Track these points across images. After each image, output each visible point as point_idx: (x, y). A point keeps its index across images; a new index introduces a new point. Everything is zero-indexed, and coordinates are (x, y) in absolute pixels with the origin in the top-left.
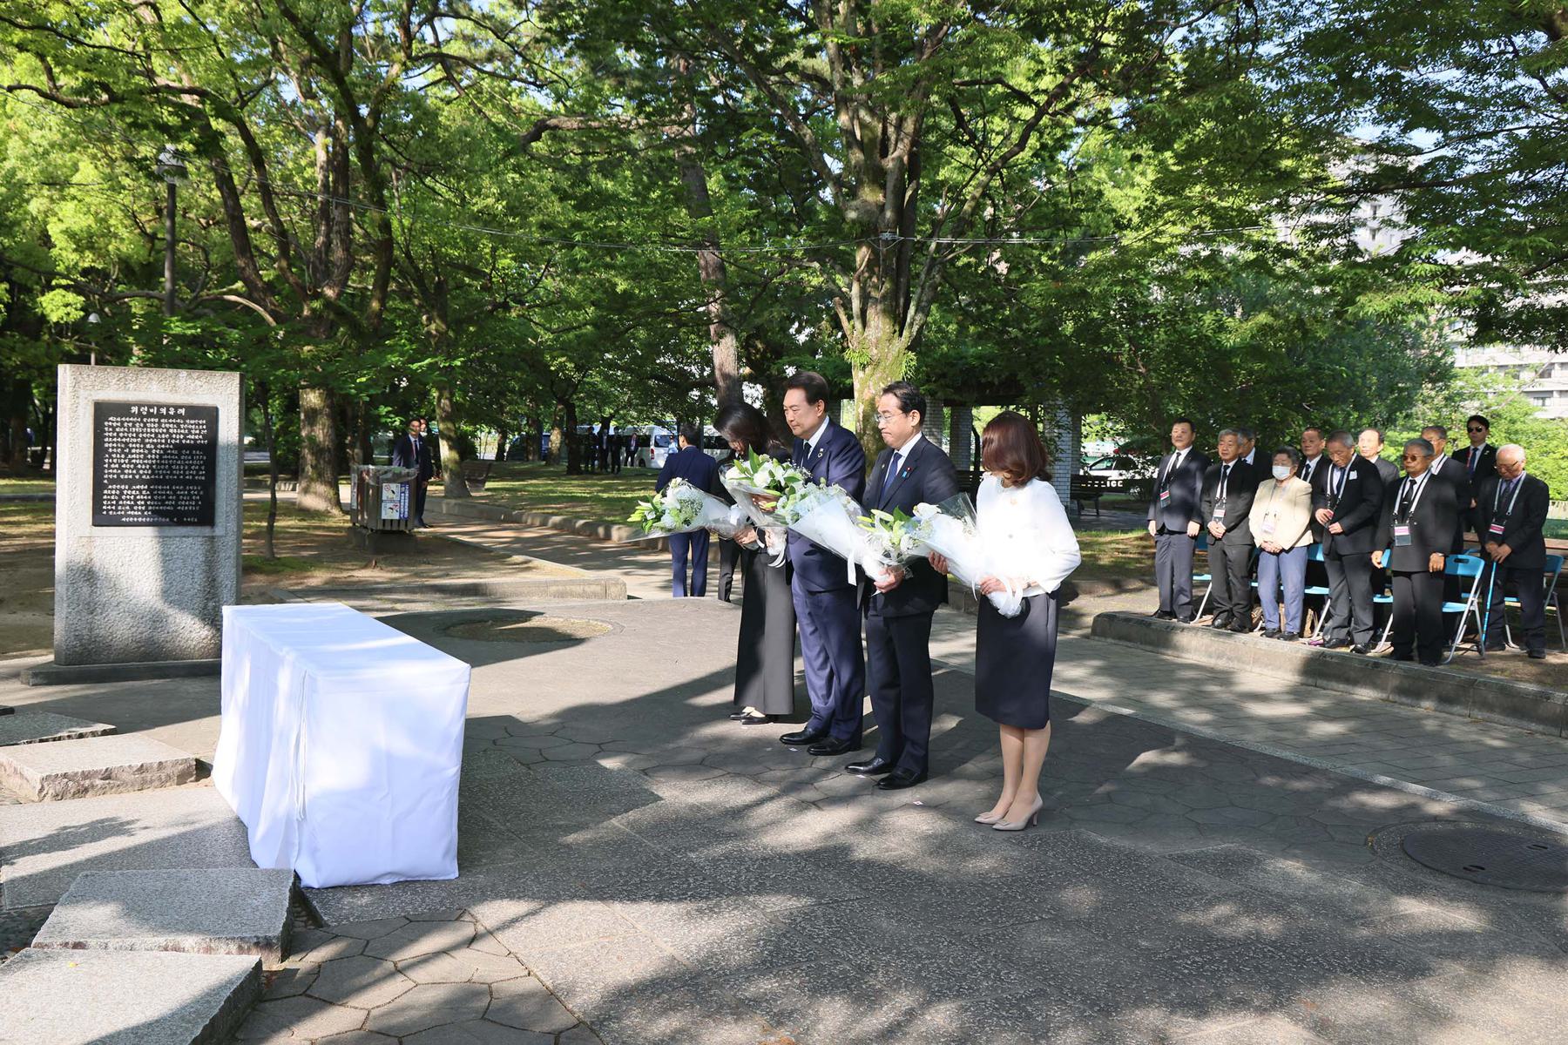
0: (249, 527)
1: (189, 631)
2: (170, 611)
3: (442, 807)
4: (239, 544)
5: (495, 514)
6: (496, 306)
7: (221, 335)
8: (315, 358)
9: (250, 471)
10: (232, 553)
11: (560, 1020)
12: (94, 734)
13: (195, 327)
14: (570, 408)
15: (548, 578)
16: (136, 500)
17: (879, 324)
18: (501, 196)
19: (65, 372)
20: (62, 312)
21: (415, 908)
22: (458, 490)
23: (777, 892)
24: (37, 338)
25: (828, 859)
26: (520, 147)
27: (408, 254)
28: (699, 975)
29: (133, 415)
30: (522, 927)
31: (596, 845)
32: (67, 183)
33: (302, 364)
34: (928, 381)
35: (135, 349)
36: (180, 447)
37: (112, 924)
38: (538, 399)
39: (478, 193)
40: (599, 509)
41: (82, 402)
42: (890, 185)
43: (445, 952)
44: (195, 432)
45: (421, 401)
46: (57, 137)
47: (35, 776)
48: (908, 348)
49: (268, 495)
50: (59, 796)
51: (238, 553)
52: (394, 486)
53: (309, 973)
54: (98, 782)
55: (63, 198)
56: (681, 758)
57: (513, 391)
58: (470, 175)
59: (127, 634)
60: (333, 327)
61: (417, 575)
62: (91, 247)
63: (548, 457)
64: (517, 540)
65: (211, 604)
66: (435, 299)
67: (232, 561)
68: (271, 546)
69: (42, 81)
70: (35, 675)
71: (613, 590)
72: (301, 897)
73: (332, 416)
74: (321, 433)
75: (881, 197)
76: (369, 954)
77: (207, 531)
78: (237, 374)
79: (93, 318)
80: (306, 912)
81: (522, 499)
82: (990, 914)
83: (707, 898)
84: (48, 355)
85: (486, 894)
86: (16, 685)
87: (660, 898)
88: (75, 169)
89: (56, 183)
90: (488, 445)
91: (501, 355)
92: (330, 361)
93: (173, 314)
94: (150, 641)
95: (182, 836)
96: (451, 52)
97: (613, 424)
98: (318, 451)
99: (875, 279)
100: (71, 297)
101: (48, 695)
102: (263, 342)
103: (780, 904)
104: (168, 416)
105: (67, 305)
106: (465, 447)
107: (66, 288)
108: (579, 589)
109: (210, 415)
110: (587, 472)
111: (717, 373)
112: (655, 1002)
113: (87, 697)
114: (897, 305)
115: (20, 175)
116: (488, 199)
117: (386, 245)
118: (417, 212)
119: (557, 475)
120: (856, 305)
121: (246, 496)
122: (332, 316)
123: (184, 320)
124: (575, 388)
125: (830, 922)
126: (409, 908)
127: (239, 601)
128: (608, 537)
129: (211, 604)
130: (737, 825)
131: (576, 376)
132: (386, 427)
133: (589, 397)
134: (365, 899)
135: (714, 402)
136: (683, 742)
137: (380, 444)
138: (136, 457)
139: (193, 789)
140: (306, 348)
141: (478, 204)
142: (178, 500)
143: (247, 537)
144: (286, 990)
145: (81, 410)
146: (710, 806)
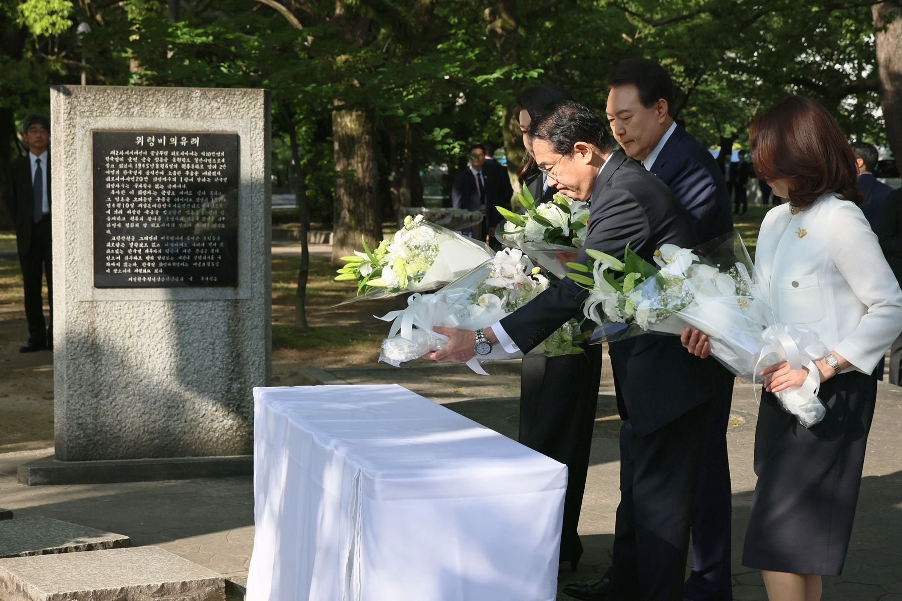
0: (276, 289)
1: (213, 419)
2: (188, 395)
4: (268, 310)
7: (237, 42)
8: (350, 69)
9: (278, 218)
10: (259, 321)
12: (105, 546)
13: (206, 34)
16: (144, 255)
19: (57, 100)
20: (46, 22)
24: (18, 56)
29: (139, 148)
33: (336, 77)
35: (134, 66)
41: (79, 132)
44: (212, 167)
45: (483, 123)
49: (298, 249)
51: (267, 322)
59: (139, 422)
60: (372, 26)
65: (236, 386)
67: (260, 332)
68: (303, 313)
70: (34, 472)
74: (359, 167)
77: (228, 292)
78: (261, 92)
79: (81, 28)
84: (32, 77)
86: (12, 484)
91: (586, 58)
92: (372, 71)
93: (178, 19)
94: (165, 431)
97: (736, 146)
98: (356, 190)
101: (32, 499)
102: (287, 50)
104: (180, 148)
105: (52, 13)
109: (229, 145)
111: (882, 72)
113: (94, 499)
121: (274, 250)
122: (371, 14)
123: (192, 25)
127: (270, 381)
129: (236, 386)
131: (686, 84)
132: (440, 158)
133: (704, 110)
135: (878, 113)
137: (431, 181)
140: (343, 57)
142: (193, 254)
143: (275, 302)
145: (78, 144)
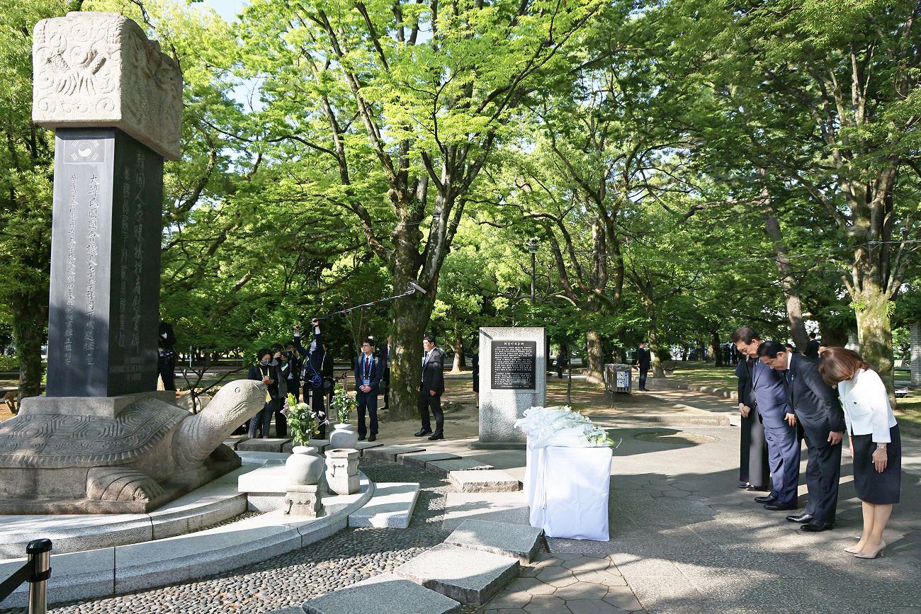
3: (601, 510)
5: (673, 386)
6: (675, 291)
11: (635, 606)
12: (486, 469)
14: (716, 336)
15: (692, 415)
17: (870, 288)
18: (672, 242)
20: (501, 306)
21: (588, 551)
22: (659, 375)
23: (760, 569)
24: (494, 316)
25: (796, 557)
26: (683, 220)
27: (634, 271)
28: (706, 600)
30: (630, 566)
31: (675, 536)
32: (501, 256)
34: (908, 316)
36: (521, 358)
37: (470, 540)
38: (701, 331)
39: (661, 243)
40: (726, 383)
42: (873, 216)
43: (594, 571)
44: (528, 353)
46: (496, 239)
47: (462, 482)
48: (890, 299)
50: (470, 491)
52: (622, 373)
53: (538, 570)
54: (483, 487)
55: (500, 262)
56: (729, 502)
57: (689, 329)
58: (657, 235)
61: (631, 412)
62: (510, 280)
63: (707, 359)
64: (683, 397)
66: (647, 289)
69: (490, 220)
71: (723, 422)
72: (543, 540)
73: (600, 343)
74: (596, 351)
75: (868, 223)
76: (564, 566)
77: (532, 391)
80: (543, 544)
81: (689, 378)
82: (881, 598)
83: (722, 567)
85: (618, 551)
86: (466, 448)
87: (698, 563)
88: (505, 250)
89: (498, 256)
90: (676, 352)
95: (507, 511)
96: (652, 183)
98: (594, 358)
99: (867, 265)
100: (504, 299)
103: (758, 575)
104: (517, 346)
106: (664, 356)
107: (502, 296)
108: (705, 421)
109: (534, 344)
110: (726, 365)
112: (681, 607)
114: (882, 277)
115: (484, 255)
116: (666, 245)
117: (621, 269)
118: (637, 253)
119: (711, 367)
120: (855, 280)
124: (719, 326)
125: (784, 587)
126: (585, 551)
128: (729, 397)
130: (750, 536)
134: (568, 545)
136: (733, 495)
138: (507, 363)
139: (517, 493)
141: (661, 247)
144: (528, 575)
146: (738, 525)
